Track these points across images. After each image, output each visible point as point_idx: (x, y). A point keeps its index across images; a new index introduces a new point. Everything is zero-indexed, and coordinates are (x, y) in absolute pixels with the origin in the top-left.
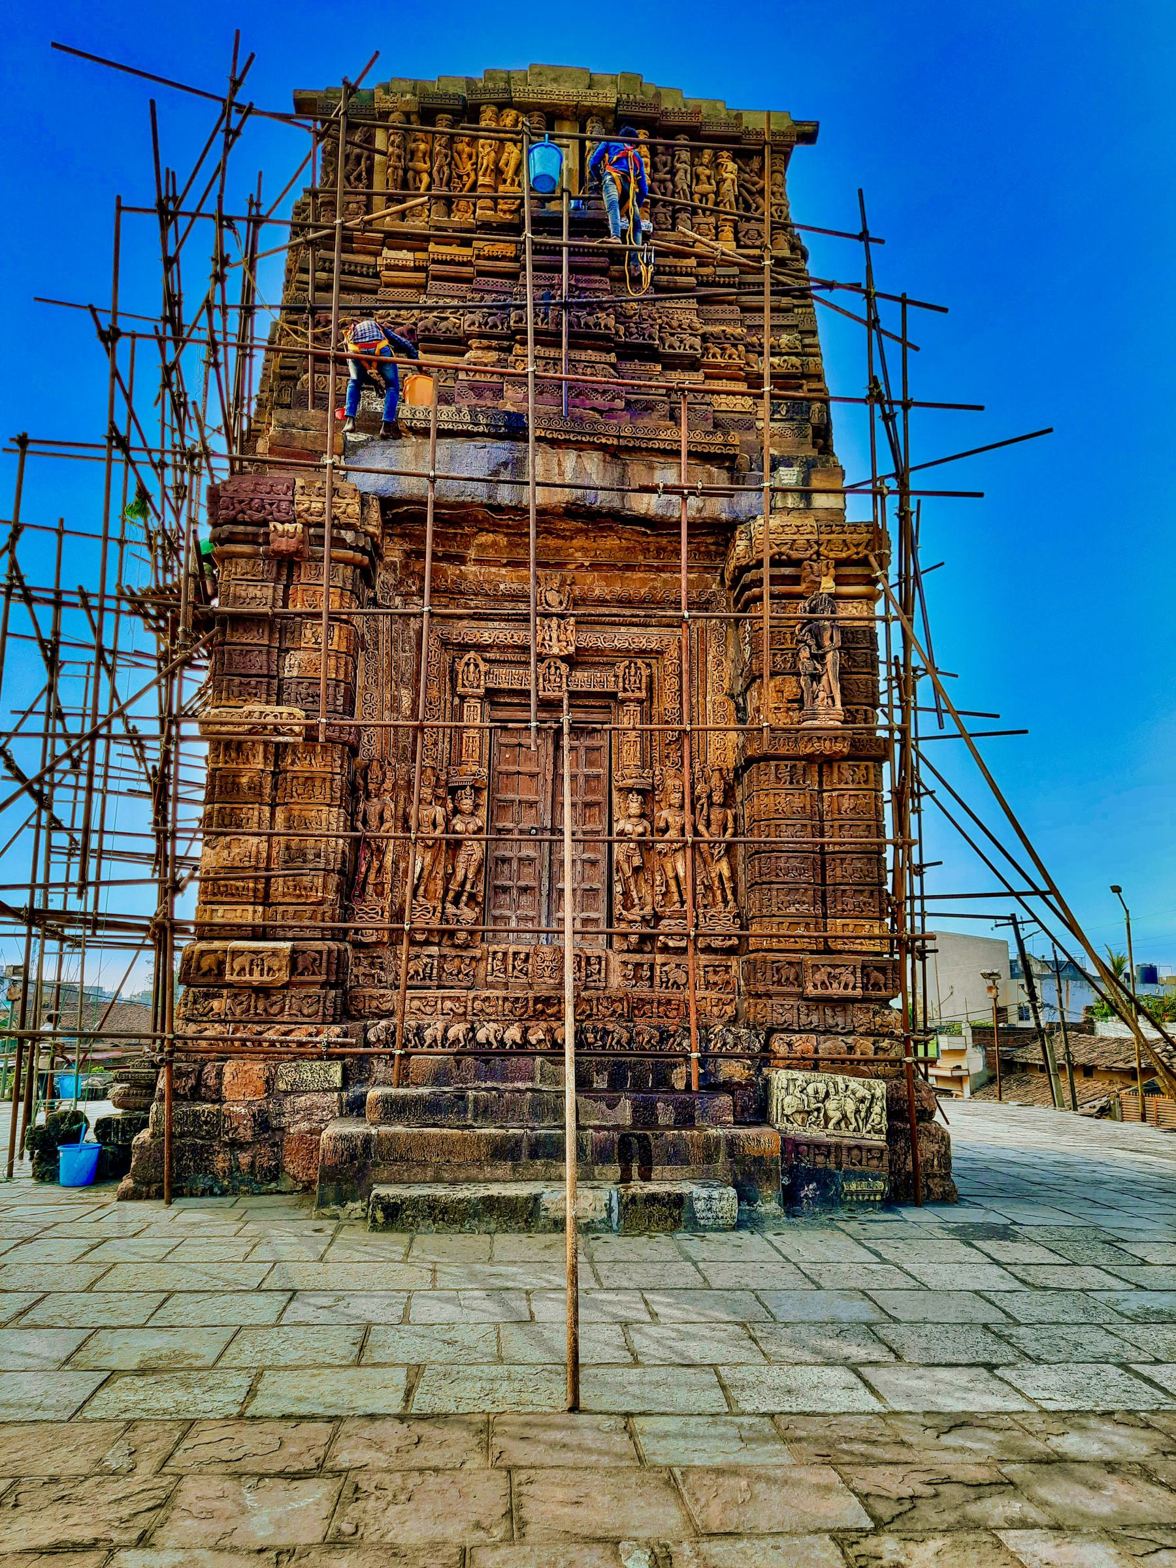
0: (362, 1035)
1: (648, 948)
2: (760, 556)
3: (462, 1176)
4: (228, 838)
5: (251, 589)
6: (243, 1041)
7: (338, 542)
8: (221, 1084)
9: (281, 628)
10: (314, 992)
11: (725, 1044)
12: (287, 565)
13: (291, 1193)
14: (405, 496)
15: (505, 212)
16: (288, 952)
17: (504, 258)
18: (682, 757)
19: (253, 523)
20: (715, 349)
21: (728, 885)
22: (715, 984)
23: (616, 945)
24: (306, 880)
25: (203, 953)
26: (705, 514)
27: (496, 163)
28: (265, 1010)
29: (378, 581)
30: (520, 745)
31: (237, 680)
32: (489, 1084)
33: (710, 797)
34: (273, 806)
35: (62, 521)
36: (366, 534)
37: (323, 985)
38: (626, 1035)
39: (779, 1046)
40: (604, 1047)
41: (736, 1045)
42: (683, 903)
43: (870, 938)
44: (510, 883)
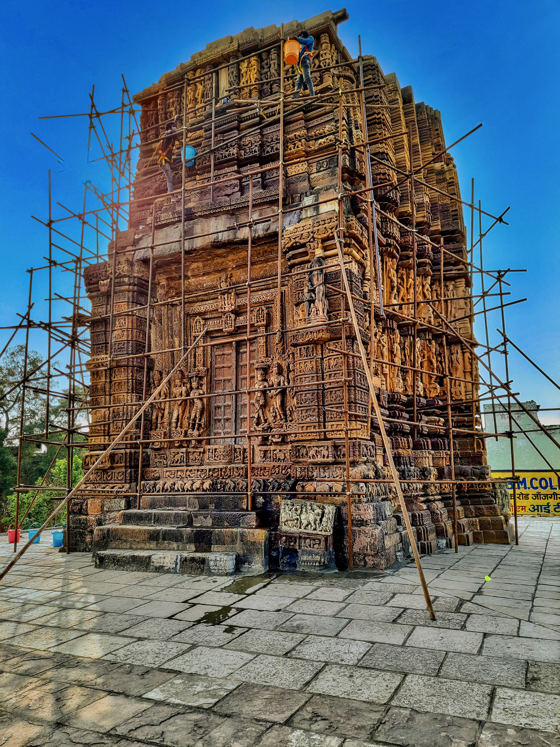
3: (139, 547)
26: (269, 231)
27: (194, 96)
30: (224, 354)
32: (170, 508)
38: (233, 485)
40: (224, 490)
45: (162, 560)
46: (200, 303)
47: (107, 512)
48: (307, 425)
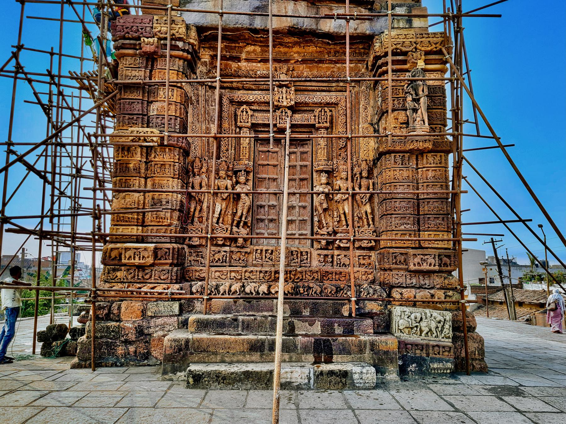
0: (189, 289)
1: (331, 247)
2: (387, 50)
4: (124, 194)
5: (133, 72)
6: (132, 292)
7: (174, 47)
8: (120, 312)
9: (148, 90)
10: (166, 268)
11: (369, 294)
12: (151, 59)
13: (155, 365)
14: (209, 25)
16: (152, 249)
18: (347, 155)
19: (133, 39)
21: (370, 217)
22: (364, 264)
24: (162, 214)
25: (112, 249)
26: (358, 31)
28: (143, 277)
29: (198, 72)
31: (127, 117)
32: (251, 313)
33: (361, 174)
34: (146, 178)
35: (52, 48)
36: (189, 44)
37: (171, 265)
38: (319, 289)
39: (396, 294)
40: (308, 295)
41: (374, 294)
42: (347, 225)
43: (442, 241)
44: (264, 217)
45: (289, 375)
46: (245, 92)
47: (152, 317)
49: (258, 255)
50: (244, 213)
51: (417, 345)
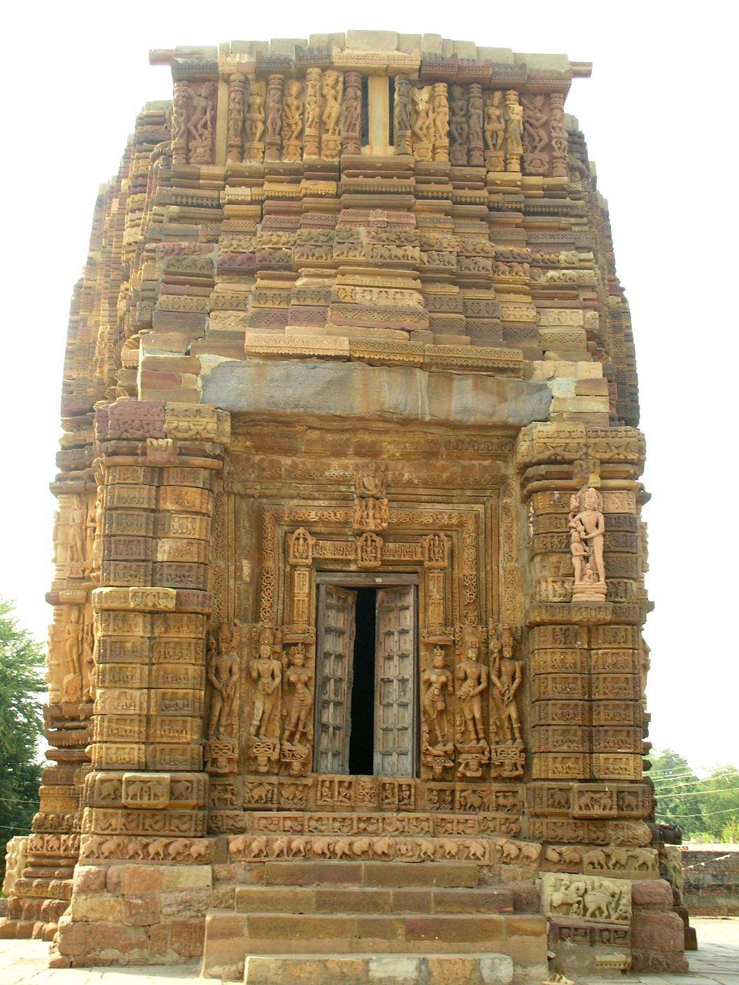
5: (131, 491)
15: (327, 156)
17: (326, 196)
20: (503, 267)
22: (504, 806)
23: (423, 776)
25: (103, 781)
33: (501, 652)
46: (302, 502)
48: (563, 755)
49: (326, 792)
50: (302, 718)
51: (576, 929)
